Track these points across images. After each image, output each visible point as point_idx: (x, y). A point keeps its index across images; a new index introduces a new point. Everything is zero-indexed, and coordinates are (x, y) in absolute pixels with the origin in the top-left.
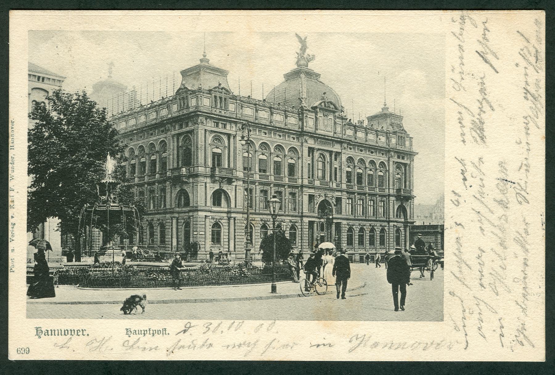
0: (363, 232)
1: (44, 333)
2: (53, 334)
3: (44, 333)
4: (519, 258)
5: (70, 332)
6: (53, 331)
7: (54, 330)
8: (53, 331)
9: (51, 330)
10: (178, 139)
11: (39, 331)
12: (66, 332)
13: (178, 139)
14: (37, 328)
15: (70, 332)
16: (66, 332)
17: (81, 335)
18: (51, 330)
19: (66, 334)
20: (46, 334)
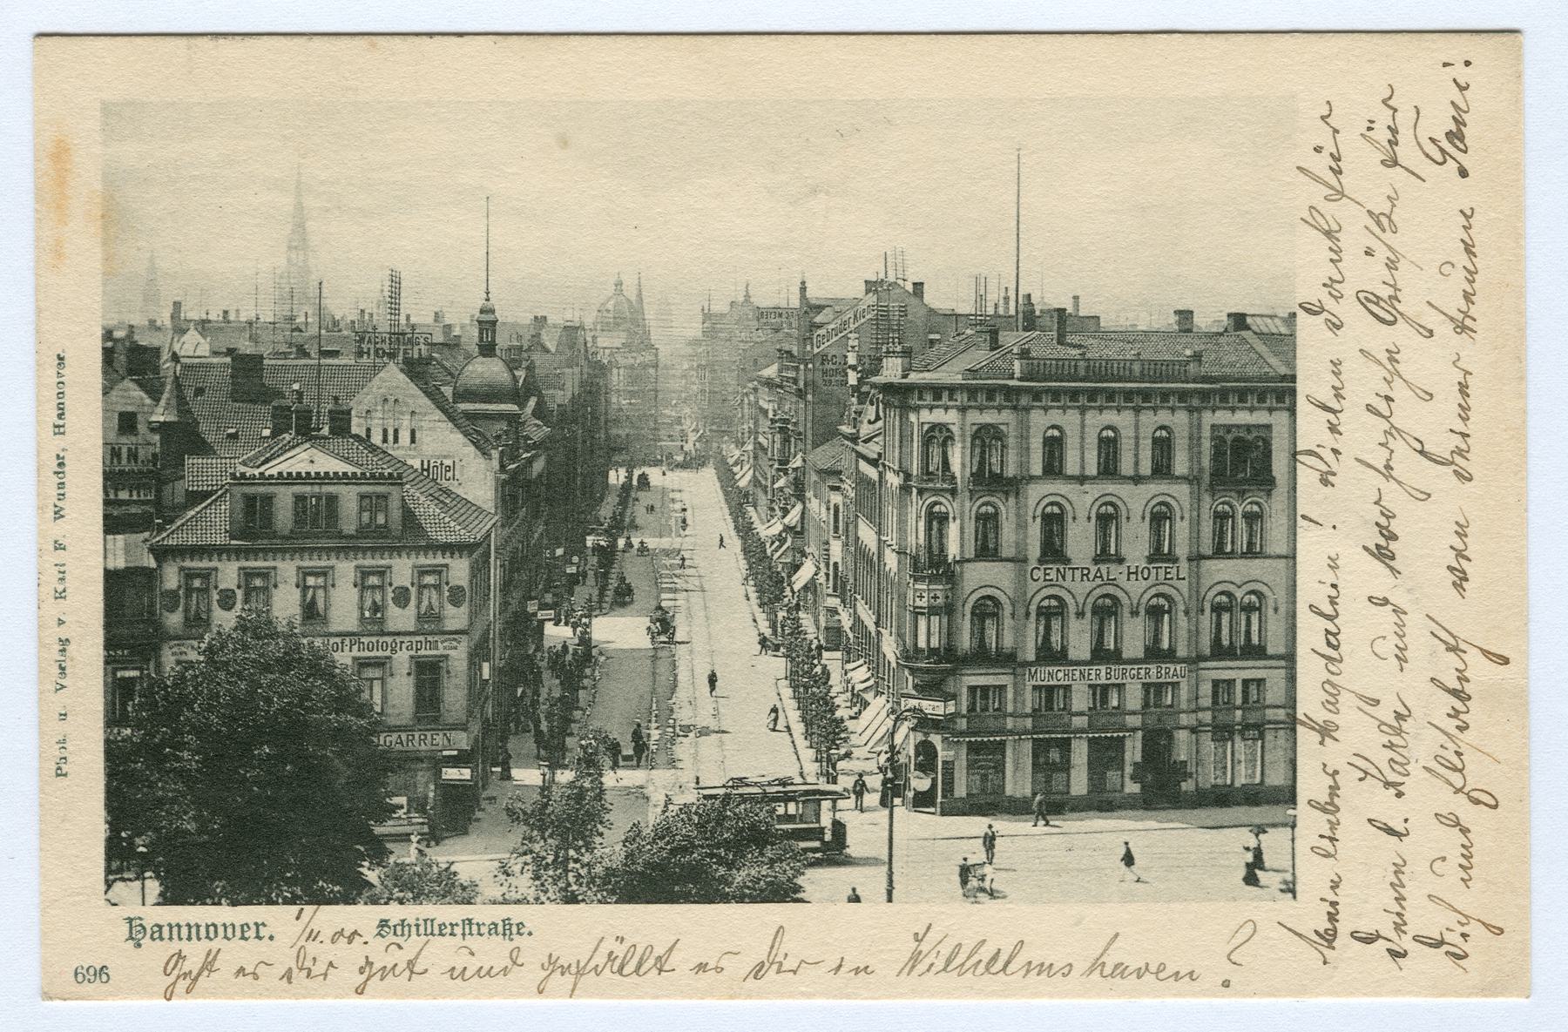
1: (149, 932)
3: (149, 932)
5: (221, 930)
15: (221, 930)
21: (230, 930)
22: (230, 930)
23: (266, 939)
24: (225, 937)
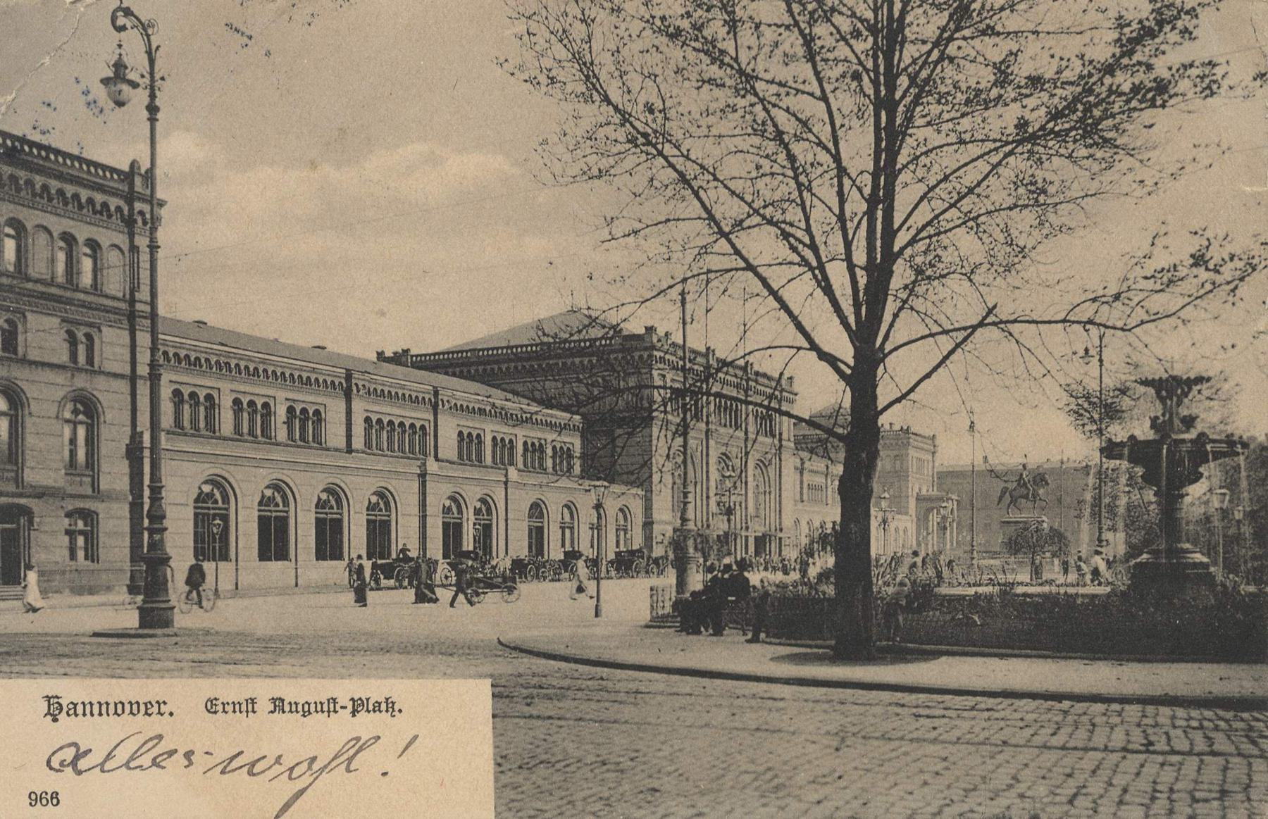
0: (541, 515)
1: (65, 709)
2: (88, 711)
3: (65, 709)
4: (785, 69)
5: (127, 707)
6: (88, 707)
7: (107, 704)
8: (88, 707)
9: (100, 703)
10: (537, 537)
11: (211, 706)
12: (119, 706)
13: (537, 537)
14: (48, 698)
15: (127, 707)
16: (119, 706)
17: (230, 713)
18: (100, 703)
19: (119, 711)
20: (72, 712)
21: (135, 707)
22: (135, 707)
23: (166, 715)
24: (131, 713)
